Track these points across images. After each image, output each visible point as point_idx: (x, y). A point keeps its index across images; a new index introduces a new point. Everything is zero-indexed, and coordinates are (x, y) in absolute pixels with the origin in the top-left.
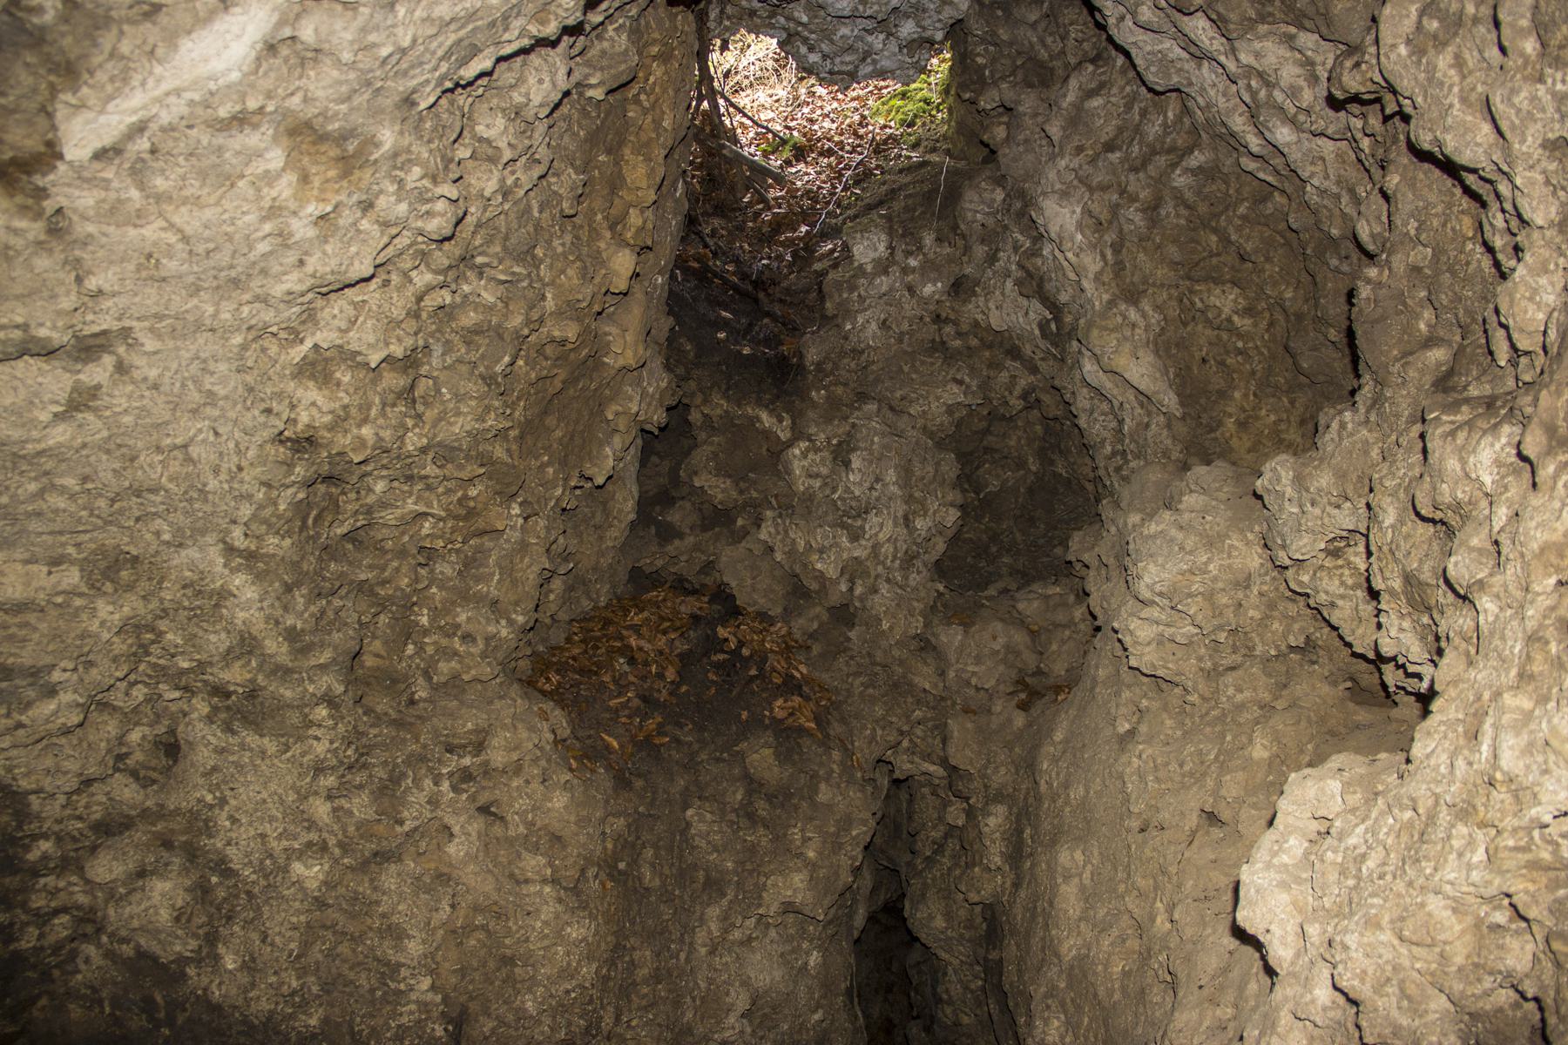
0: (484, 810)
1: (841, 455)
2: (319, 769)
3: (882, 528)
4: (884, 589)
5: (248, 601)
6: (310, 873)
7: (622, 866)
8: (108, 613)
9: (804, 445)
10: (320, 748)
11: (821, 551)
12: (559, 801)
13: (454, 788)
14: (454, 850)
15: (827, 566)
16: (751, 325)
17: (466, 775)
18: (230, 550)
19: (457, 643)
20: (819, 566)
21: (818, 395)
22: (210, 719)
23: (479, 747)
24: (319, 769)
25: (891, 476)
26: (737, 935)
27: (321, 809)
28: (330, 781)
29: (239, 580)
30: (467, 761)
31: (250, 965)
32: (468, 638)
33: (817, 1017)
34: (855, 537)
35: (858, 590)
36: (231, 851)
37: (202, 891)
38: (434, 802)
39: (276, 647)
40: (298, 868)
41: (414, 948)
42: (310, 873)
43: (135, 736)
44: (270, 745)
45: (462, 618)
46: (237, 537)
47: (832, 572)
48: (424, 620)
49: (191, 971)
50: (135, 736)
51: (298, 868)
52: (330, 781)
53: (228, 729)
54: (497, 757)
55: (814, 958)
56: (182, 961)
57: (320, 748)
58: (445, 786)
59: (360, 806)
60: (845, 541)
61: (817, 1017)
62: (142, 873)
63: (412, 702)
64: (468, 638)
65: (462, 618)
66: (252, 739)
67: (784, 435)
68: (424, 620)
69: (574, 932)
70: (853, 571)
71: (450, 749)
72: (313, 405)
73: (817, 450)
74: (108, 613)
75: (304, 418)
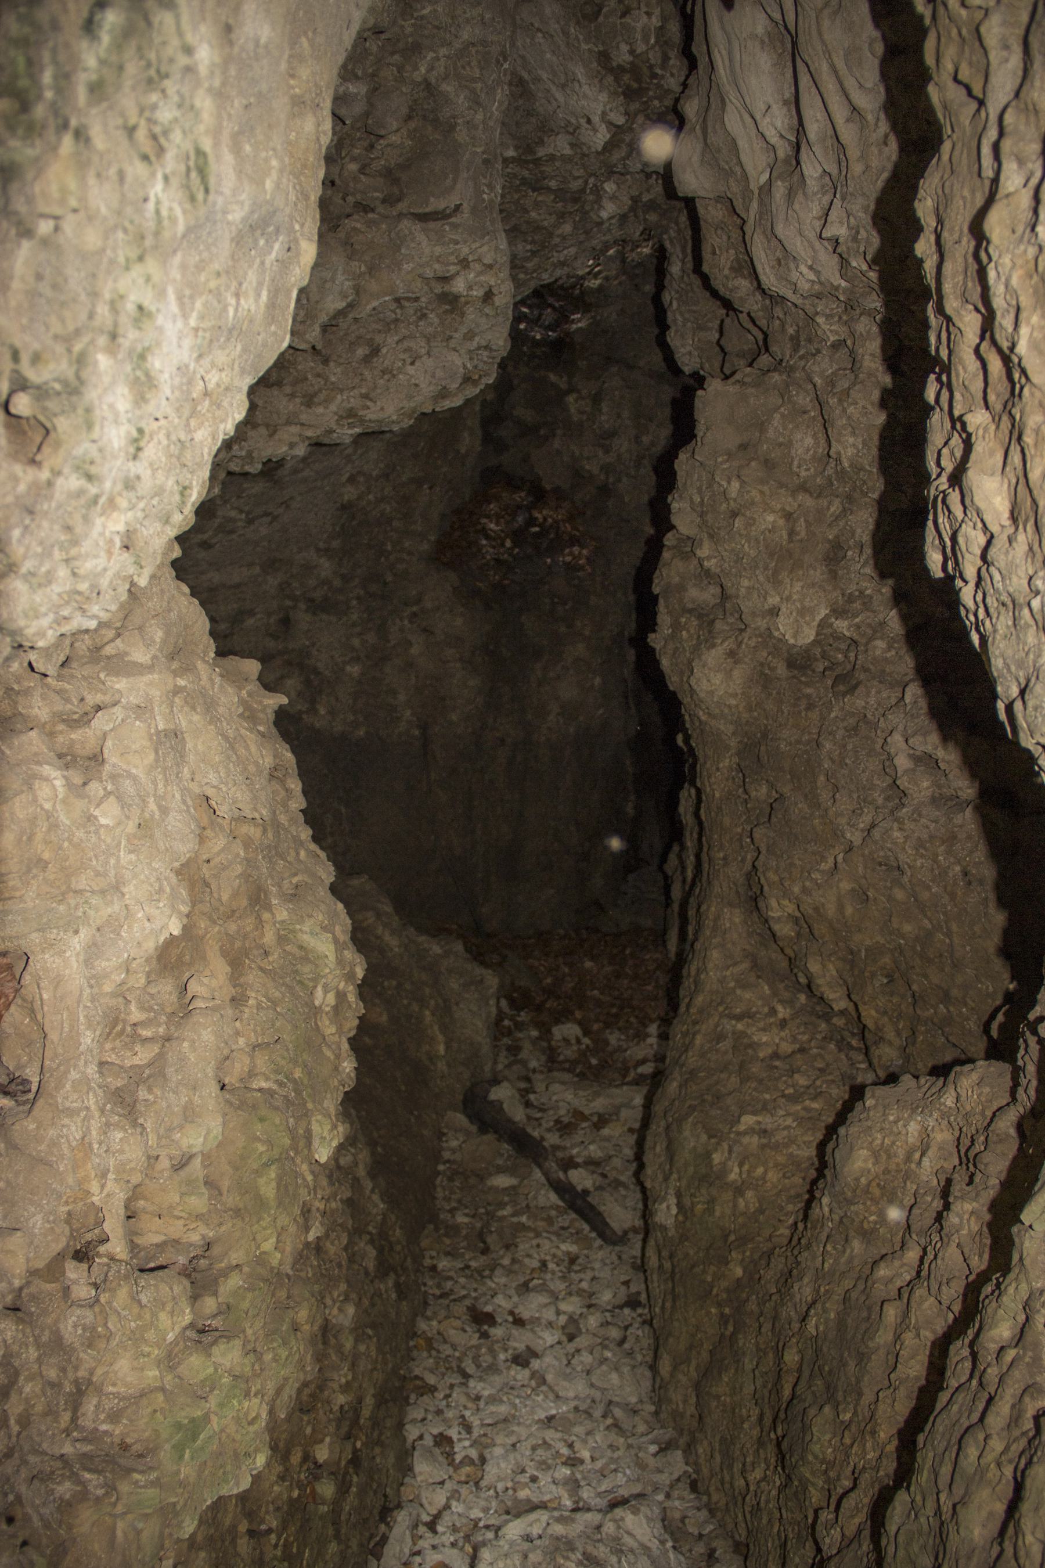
0: (425, 630)
1: (597, 399)
2: (354, 625)
3: (623, 445)
4: (625, 480)
5: (326, 567)
6: (354, 670)
7: (491, 647)
8: (273, 582)
9: (575, 395)
10: (355, 617)
11: (588, 458)
12: (459, 621)
13: (411, 622)
14: (415, 650)
15: (592, 467)
16: (540, 315)
17: (415, 615)
18: (318, 550)
19: (405, 556)
20: (587, 467)
21: (582, 364)
22: (306, 611)
23: (419, 601)
24: (354, 625)
25: (626, 414)
26: (552, 674)
27: (356, 642)
28: (358, 629)
29: (322, 560)
30: (414, 609)
31: (332, 712)
32: (410, 553)
33: (601, 711)
34: (607, 450)
35: (611, 480)
36: (319, 664)
37: (308, 682)
38: (402, 630)
39: (337, 583)
40: (348, 668)
41: (402, 698)
42: (354, 670)
43: (272, 620)
44: (333, 619)
45: (407, 544)
46: (321, 545)
47: (596, 471)
48: (389, 548)
49: (304, 716)
50: (272, 620)
51: (348, 668)
52: (358, 629)
53: (314, 614)
54: (429, 605)
55: (598, 681)
56: (300, 712)
57: (355, 617)
58: (406, 622)
59: (371, 638)
60: (600, 453)
61: (601, 711)
62: (282, 677)
63: (385, 584)
64: (410, 553)
65: (407, 544)
66: (324, 617)
67: (563, 386)
68: (389, 548)
69: (471, 683)
70: (606, 469)
71: (406, 604)
72: (350, 493)
73: (583, 398)
74: (273, 582)
75: (346, 498)
